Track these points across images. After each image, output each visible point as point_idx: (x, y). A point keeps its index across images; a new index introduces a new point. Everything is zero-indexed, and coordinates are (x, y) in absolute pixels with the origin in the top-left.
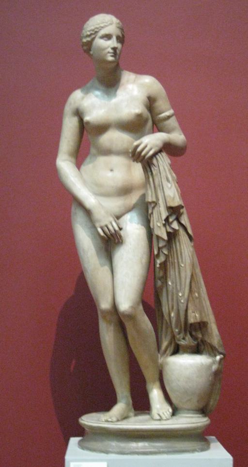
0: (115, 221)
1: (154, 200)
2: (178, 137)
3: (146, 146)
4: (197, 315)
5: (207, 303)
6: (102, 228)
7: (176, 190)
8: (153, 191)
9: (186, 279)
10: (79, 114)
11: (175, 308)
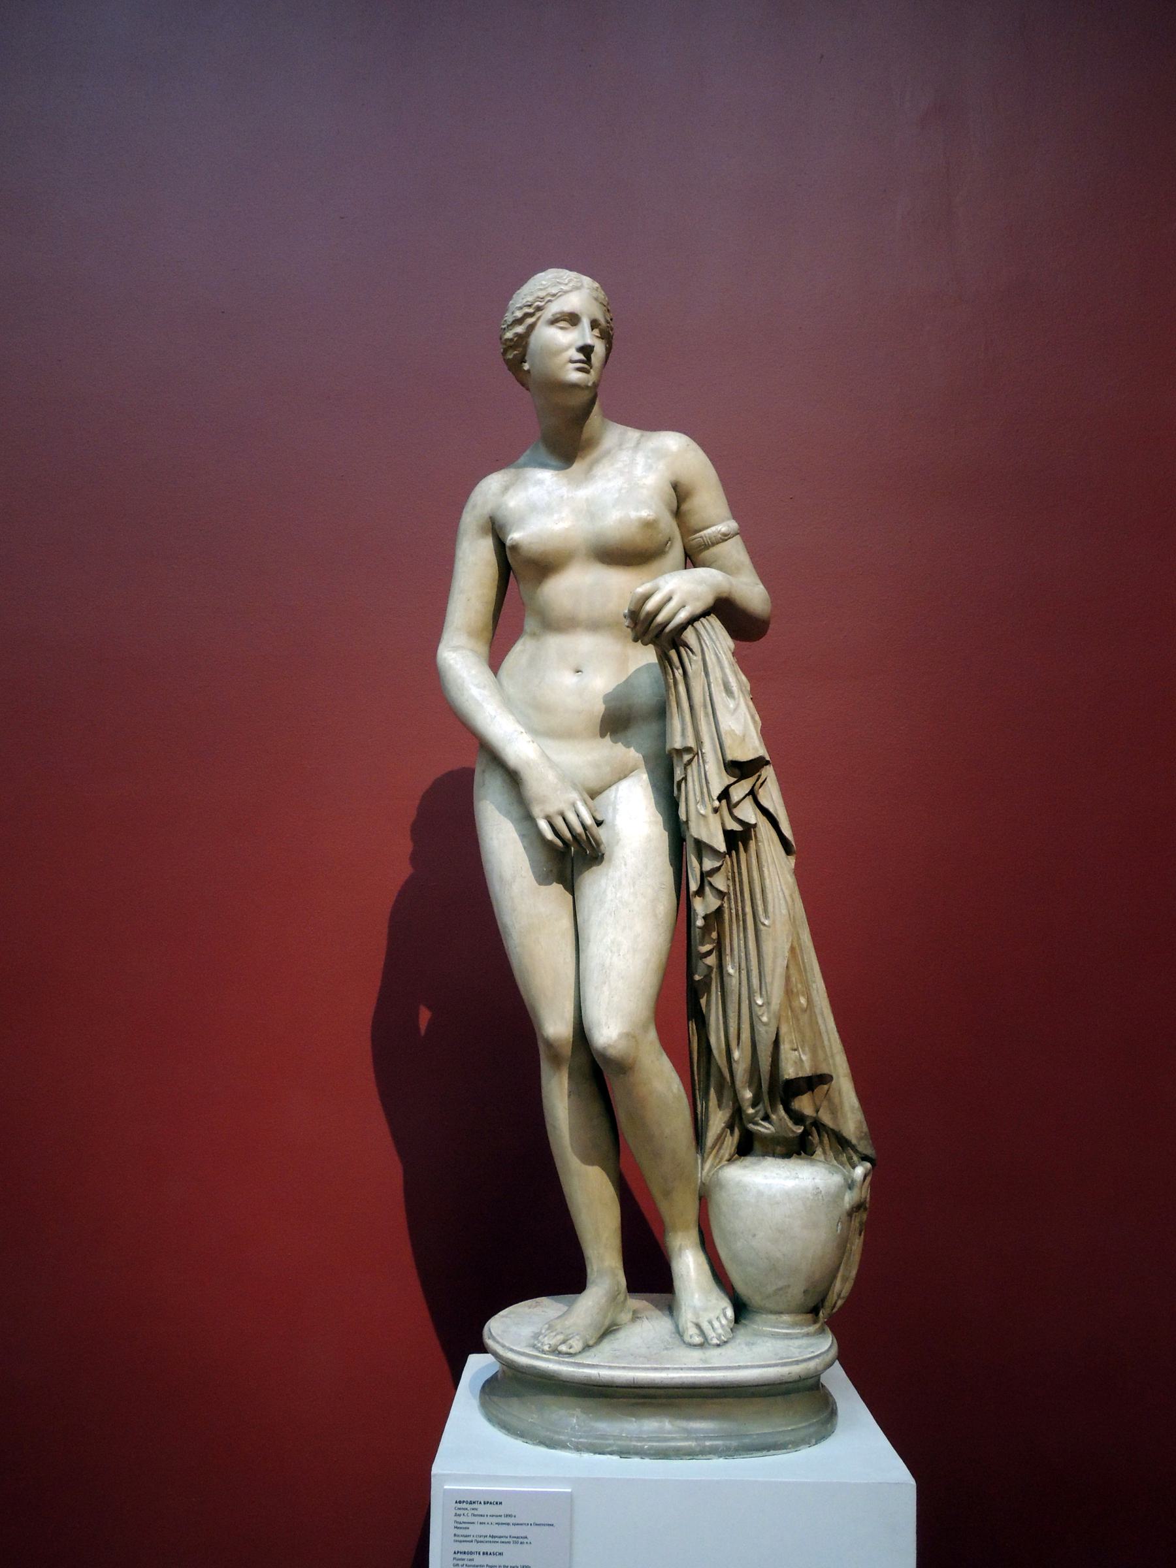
1: (691, 743)
2: (752, 592)
4: (804, 1058)
7: (749, 717)
10: (496, 529)
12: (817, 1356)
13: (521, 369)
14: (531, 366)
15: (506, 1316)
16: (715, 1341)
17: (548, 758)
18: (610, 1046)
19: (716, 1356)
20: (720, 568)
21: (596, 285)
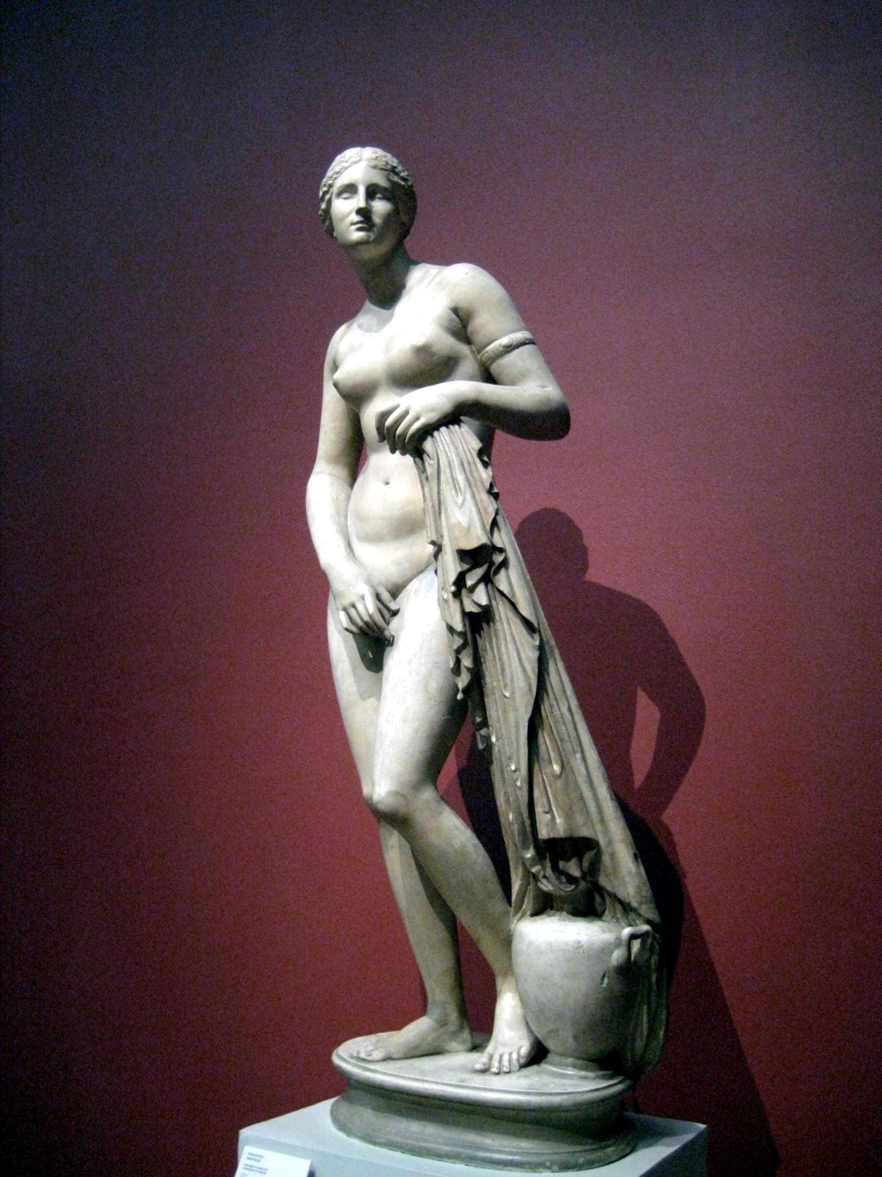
3: (406, 413)
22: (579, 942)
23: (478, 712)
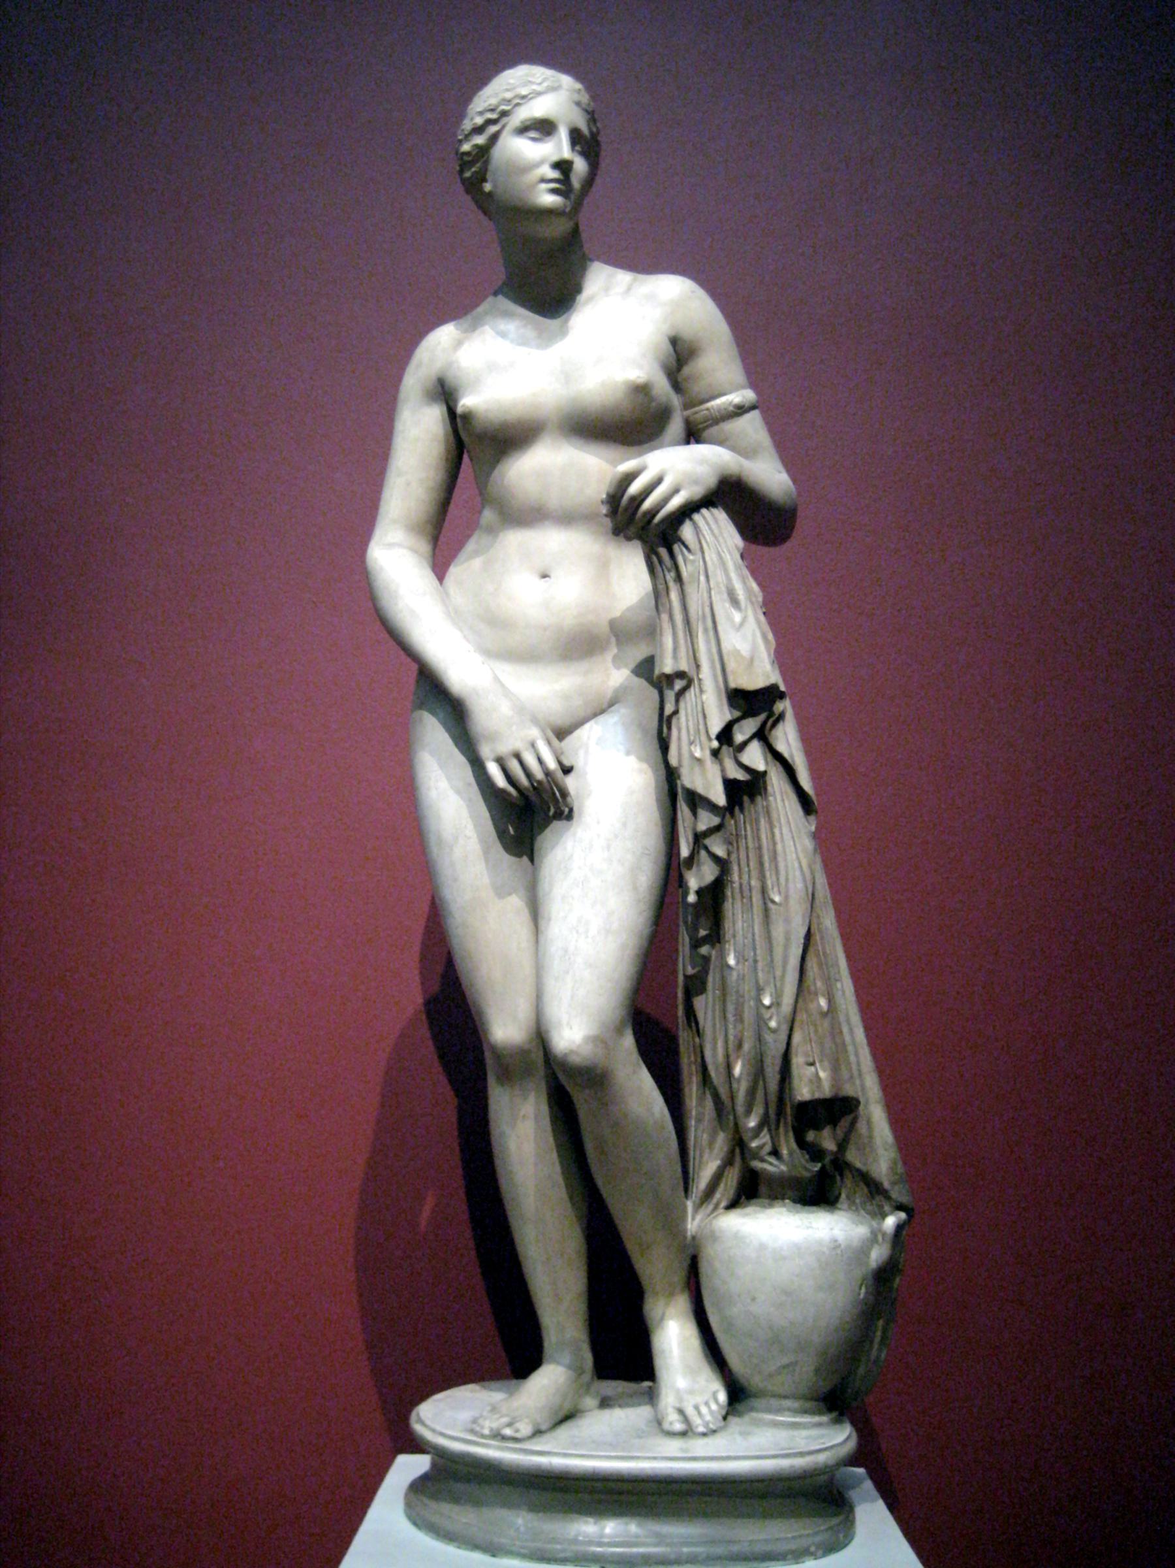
0: (549, 743)
1: (684, 666)
2: (770, 475)
3: (659, 481)
4: (822, 1074)
5: (856, 1034)
6: (500, 761)
7: (758, 634)
8: (681, 634)
9: (786, 947)
10: (444, 393)
11: (746, 1046)
12: (832, 1447)
13: (481, 190)
14: (495, 186)
15: (440, 1400)
16: (701, 1429)
17: (502, 685)
18: (572, 1052)
19: (699, 1446)
20: (733, 449)
21: (578, 86)
22: (836, 1241)
23: (703, 920)
